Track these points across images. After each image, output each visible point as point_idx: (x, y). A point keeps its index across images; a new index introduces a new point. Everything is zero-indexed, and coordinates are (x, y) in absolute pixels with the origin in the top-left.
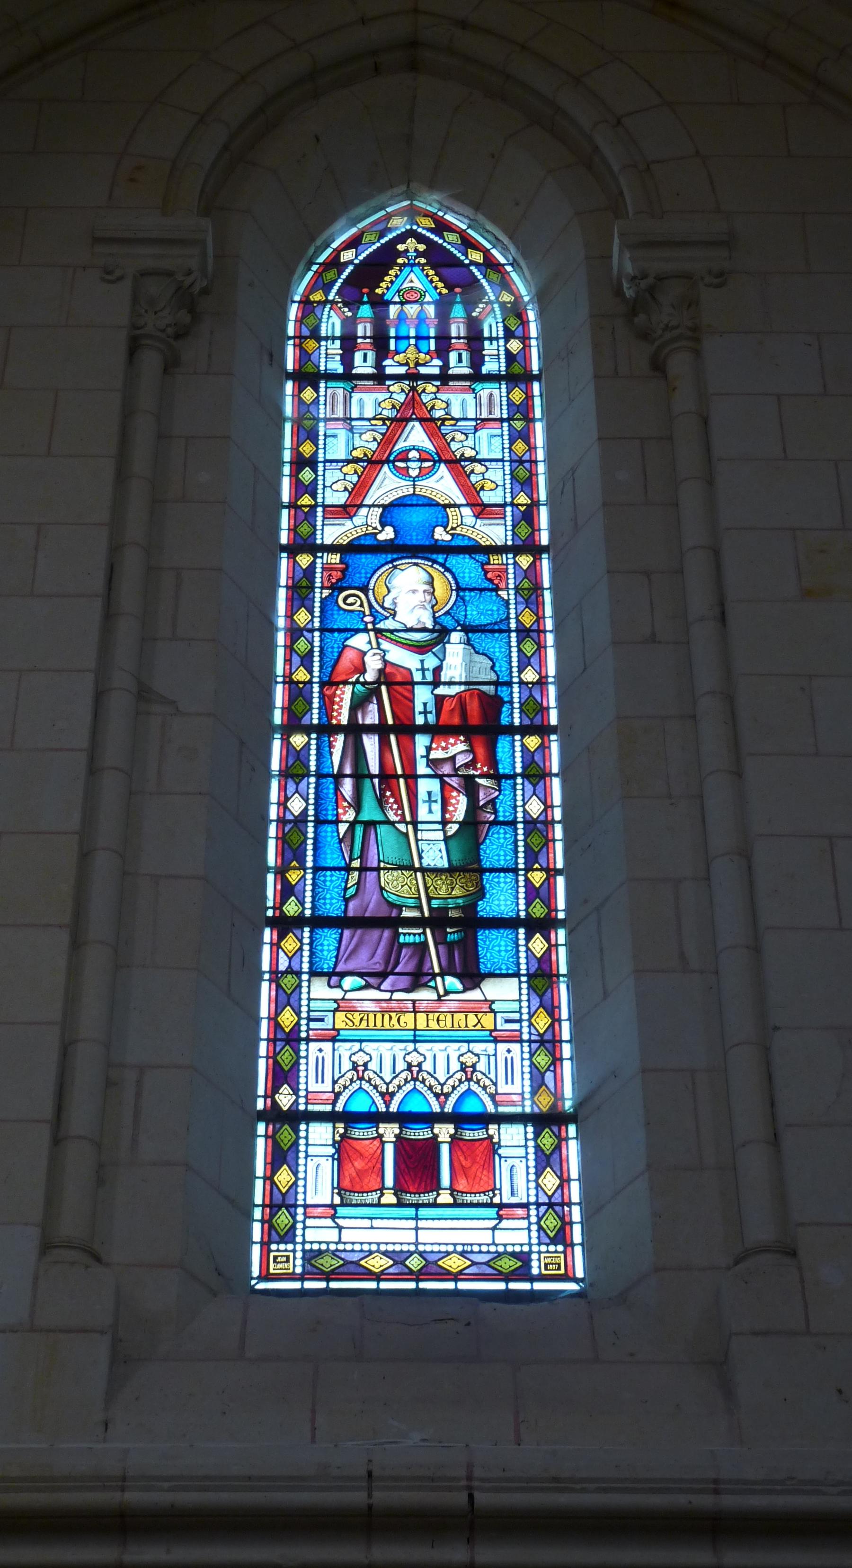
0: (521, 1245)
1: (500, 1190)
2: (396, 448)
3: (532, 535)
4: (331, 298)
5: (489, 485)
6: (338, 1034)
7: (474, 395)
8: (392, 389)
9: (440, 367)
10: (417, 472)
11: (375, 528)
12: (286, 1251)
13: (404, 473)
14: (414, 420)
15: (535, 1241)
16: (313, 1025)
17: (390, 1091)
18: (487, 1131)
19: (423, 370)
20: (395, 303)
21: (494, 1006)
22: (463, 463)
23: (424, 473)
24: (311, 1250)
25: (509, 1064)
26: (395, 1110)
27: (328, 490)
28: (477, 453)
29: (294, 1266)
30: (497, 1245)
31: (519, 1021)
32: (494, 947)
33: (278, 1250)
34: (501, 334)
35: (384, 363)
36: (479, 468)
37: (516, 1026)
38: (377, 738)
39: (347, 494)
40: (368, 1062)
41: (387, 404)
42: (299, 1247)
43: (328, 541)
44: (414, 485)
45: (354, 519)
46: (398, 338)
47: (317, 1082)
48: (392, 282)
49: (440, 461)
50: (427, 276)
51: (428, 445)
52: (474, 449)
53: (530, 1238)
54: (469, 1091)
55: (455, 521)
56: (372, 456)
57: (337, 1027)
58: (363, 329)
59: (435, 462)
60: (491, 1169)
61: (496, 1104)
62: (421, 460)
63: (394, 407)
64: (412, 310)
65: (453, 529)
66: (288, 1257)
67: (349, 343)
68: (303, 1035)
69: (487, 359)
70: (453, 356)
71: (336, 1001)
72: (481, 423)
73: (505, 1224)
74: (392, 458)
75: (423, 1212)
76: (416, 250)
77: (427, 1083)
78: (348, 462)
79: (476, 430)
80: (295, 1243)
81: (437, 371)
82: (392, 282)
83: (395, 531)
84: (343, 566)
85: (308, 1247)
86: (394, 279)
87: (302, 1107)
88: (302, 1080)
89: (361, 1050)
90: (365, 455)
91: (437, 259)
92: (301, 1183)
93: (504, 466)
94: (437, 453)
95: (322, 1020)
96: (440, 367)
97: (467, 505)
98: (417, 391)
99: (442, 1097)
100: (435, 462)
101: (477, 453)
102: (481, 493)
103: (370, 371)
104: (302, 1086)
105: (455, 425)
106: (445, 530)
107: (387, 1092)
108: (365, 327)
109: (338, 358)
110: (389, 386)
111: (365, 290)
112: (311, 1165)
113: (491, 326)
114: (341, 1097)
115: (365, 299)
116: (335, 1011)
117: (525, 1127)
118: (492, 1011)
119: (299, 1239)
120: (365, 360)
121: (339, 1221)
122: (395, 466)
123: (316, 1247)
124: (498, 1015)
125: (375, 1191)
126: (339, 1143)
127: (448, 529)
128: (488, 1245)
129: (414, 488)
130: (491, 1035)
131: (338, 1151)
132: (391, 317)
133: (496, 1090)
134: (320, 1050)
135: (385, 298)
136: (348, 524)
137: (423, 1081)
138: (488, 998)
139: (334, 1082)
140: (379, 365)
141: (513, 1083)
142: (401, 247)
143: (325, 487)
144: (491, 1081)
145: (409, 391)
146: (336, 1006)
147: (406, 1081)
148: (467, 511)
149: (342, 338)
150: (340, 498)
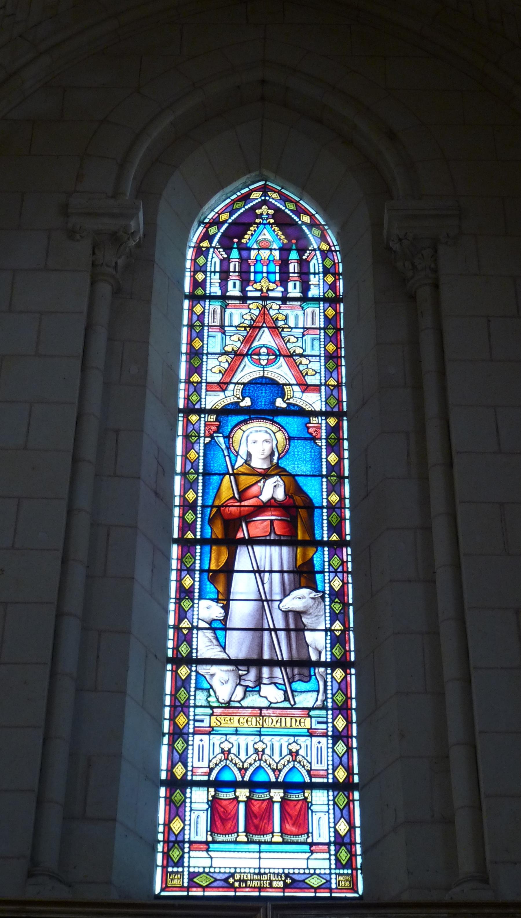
0: (325, 869)
1: (312, 833)
4: (213, 245)
5: (311, 372)
11: (239, 398)
13: (258, 362)
16: (197, 724)
20: (254, 249)
23: (270, 363)
27: (209, 372)
30: (309, 869)
31: (326, 723)
36: (304, 361)
37: (324, 726)
41: (248, 317)
43: (208, 407)
44: (264, 370)
45: (226, 392)
47: (318, 763)
48: (252, 235)
50: (274, 231)
52: (302, 348)
53: (330, 864)
61: (311, 777)
64: (264, 254)
65: (288, 399)
69: (312, 287)
73: (315, 856)
74: (250, 353)
76: (268, 214)
79: (304, 335)
90: (233, 350)
91: (281, 221)
94: (279, 350)
97: (297, 384)
98: (267, 309)
99: (243, 770)
102: (306, 377)
107: (243, 768)
109: (218, 285)
113: (314, 264)
115: (235, 246)
119: (186, 864)
122: (251, 358)
123: (196, 870)
127: (285, 399)
128: (304, 869)
133: (311, 767)
135: (248, 245)
139: (210, 761)
141: (321, 763)
142: (258, 212)
143: (207, 370)
145: (262, 308)
146: (211, 712)
147: (221, 761)
148: (296, 388)
150: (217, 378)
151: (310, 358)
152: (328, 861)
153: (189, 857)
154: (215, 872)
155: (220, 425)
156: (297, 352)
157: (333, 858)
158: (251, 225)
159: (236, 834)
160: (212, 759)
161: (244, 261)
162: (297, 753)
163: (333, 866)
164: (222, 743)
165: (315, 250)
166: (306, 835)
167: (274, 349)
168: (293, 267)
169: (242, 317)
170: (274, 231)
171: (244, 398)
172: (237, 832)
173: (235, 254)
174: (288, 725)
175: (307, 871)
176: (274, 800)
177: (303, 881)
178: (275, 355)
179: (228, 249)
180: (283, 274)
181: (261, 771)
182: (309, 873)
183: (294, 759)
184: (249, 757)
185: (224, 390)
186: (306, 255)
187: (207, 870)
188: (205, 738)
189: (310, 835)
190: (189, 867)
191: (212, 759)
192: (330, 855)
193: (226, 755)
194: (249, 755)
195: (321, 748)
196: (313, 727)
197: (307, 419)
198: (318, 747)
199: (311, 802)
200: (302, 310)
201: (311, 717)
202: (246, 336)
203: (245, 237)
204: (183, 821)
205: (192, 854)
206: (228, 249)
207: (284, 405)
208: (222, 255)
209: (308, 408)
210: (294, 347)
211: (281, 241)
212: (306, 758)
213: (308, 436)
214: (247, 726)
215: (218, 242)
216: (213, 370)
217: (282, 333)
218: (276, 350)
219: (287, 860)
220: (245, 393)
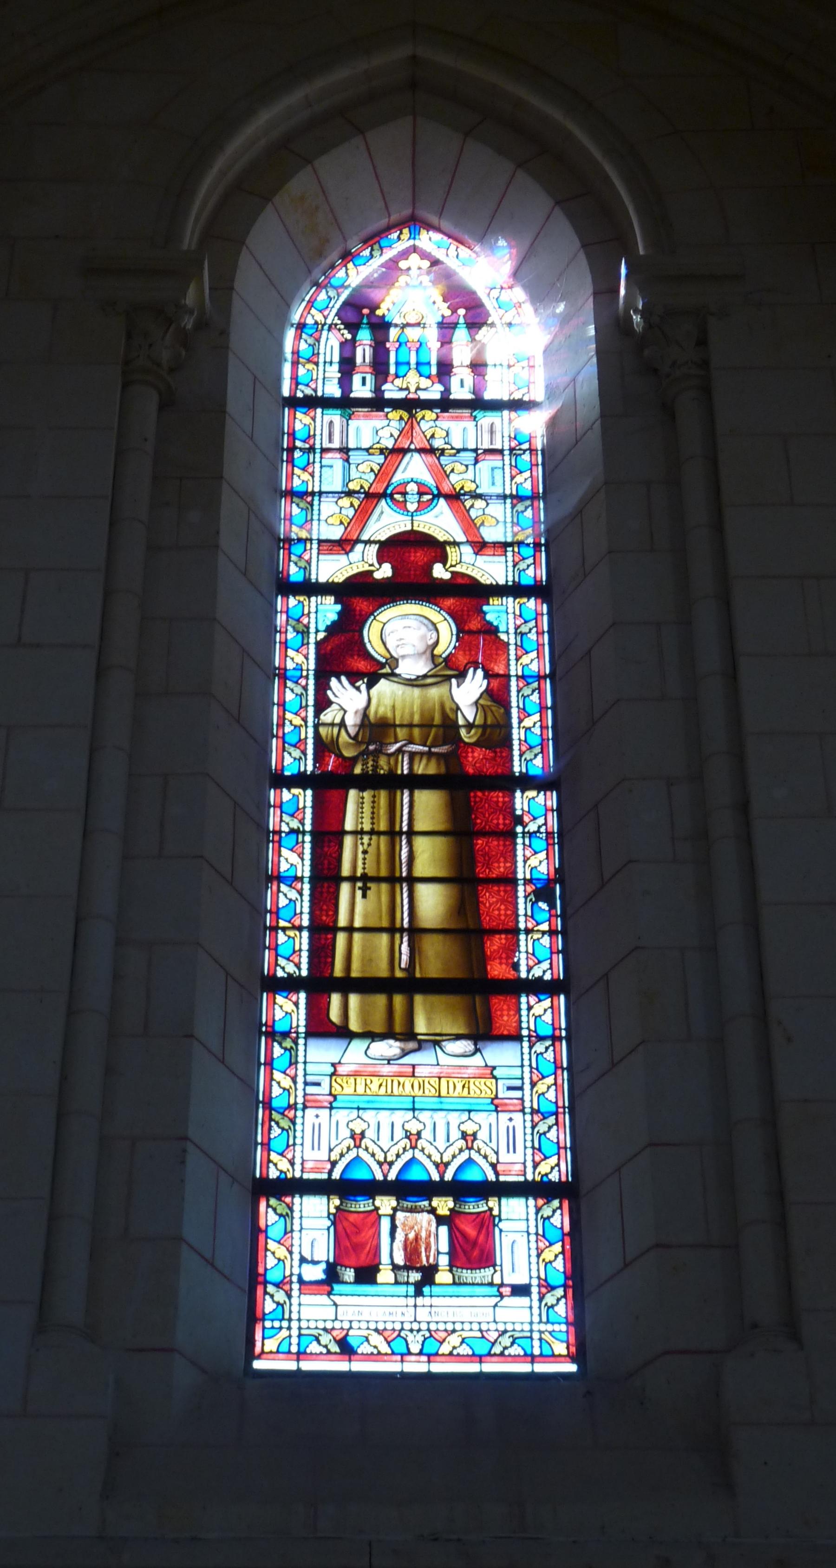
1: (501, 1266)
2: (394, 480)
8: (390, 416)
9: (442, 392)
10: (416, 505)
13: (402, 506)
14: (412, 451)
15: (536, 1319)
16: (310, 1090)
17: (389, 1159)
18: (487, 1204)
19: (423, 395)
20: (396, 325)
21: (495, 1073)
22: (462, 497)
23: (422, 507)
25: (511, 1133)
26: (338, 1178)
27: (323, 523)
28: (477, 487)
31: (521, 1088)
35: (383, 388)
36: (480, 504)
37: (518, 1094)
39: (342, 528)
43: (322, 579)
44: (412, 520)
45: (351, 554)
47: (508, 1152)
49: (440, 495)
51: (429, 480)
52: (474, 482)
54: (413, 1160)
56: (369, 488)
58: (363, 353)
59: (434, 496)
61: (497, 1174)
62: (420, 494)
67: (347, 366)
70: (454, 382)
72: (479, 454)
74: (389, 492)
79: (477, 461)
81: (437, 396)
87: (298, 1174)
90: (362, 487)
94: (437, 487)
95: (318, 1084)
96: (442, 392)
98: (416, 419)
101: (477, 487)
103: (369, 395)
105: (455, 455)
106: (444, 566)
108: (364, 350)
109: (336, 381)
110: (388, 413)
114: (337, 1166)
115: (365, 321)
116: (332, 1075)
117: (527, 1199)
118: (494, 1077)
120: (364, 383)
121: (336, 1299)
126: (334, 1215)
127: (448, 565)
129: (412, 523)
130: (492, 1103)
131: (334, 1223)
132: (391, 339)
133: (498, 1159)
134: (317, 1116)
136: (342, 559)
137: (479, 1151)
139: (331, 1150)
140: (378, 390)
141: (514, 1152)
142: (403, 264)
145: (408, 419)
146: (332, 1070)
147: (461, 1150)
148: (467, 550)
150: (336, 533)
156: (466, 489)
171: (380, 564)
176: (380, 1212)
178: (429, 496)
179: (353, 327)
183: (358, 1143)
187: (329, 1325)
189: (498, 1268)
195: (514, 1128)
198: (508, 1128)
199: (499, 1216)
205: (305, 1299)
206: (353, 327)
207: (447, 576)
209: (485, 580)
215: (337, 315)
216: (330, 521)
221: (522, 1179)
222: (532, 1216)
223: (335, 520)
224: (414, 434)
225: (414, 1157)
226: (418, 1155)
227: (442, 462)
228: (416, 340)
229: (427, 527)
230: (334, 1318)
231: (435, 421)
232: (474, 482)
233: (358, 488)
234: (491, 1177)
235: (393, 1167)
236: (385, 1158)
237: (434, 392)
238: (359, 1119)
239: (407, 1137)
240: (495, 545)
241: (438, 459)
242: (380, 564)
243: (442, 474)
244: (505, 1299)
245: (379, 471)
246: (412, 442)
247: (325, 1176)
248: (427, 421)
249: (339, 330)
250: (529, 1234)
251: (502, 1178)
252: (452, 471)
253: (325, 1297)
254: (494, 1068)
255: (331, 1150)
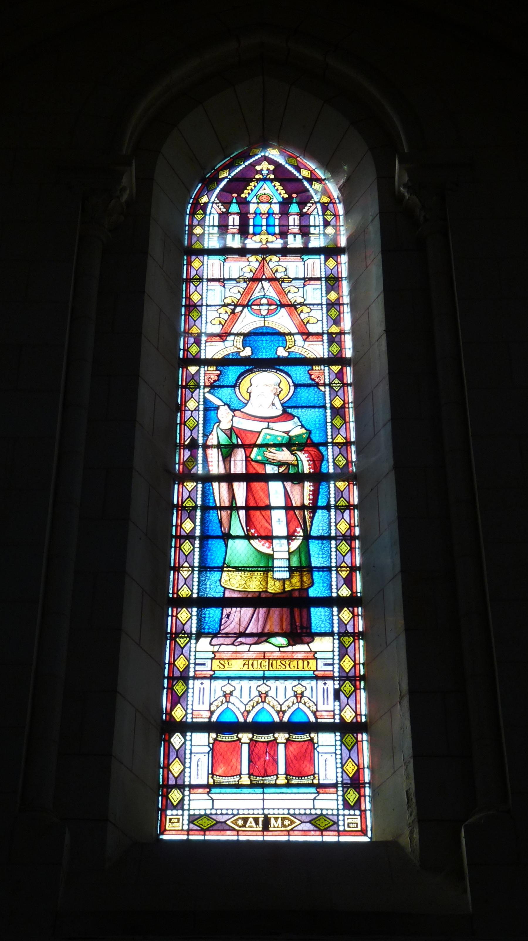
0: (332, 810)
1: (318, 774)
3: (340, 351)
4: (212, 200)
6: (214, 674)
7: (303, 263)
8: (250, 259)
11: (238, 349)
12: (177, 815)
13: (259, 313)
16: (198, 668)
19: (270, 246)
21: (316, 656)
23: (270, 313)
24: (194, 815)
27: (209, 324)
29: (183, 825)
30: (316, 809)
31: (333, 664)
32: (319, 617)
33: (172, 815)
34: (322, 223)
36: (306, 309)
37: (330, 668)
38: (245, 483)
40: (267, 692)
41: (247, 269)
42: (186, 813)
43: (209, 356)
44: (264, 320)
45: (226, 342)
46: (254, 226)
47: (324, 704)
50: (275, 186)
52: (303, 297)
53: (338, 805)
55: (291, 343)
56: (237, 302)
57: (213, 669)
58: (234, 220)
60: (312, 761)
61: (316, 718)
63: (251, 271)
64: (264, 208)
66: (179, 819)
67: (223, 227)
68: (191, 674)
71: (213, 652)
72: (307, 280)
73: (321, 796)
74: (250, 304)
75: (266, 790)
76: (268, 170)
77: (307, 705)
78: (223, 306)
79: (304, 286)
80: (183, 810)
82: (252, 190)
83: (252, 350)
84: (219, 372)
85: (192, 812)
86: (253, 188)
87: (189, 720)
88: (190, 703)
89: (299, 684)
91: (281, 175)
92: (187, 770)
93: (322, 308)
94: (280, 301)
95: (204, 664)
98: (266, 261)
100: (278, 305)
102: (308, 325)
104: (190, 707)
107: (281, 711)
111: (235, 195)
112: (194, 759)
115: (234, 201)
116: (212, 659)
119: (186, 807)
121: (214, 796)
122: (251, 308)
123: (197, 812)
124: (318, 660)
125: (236, 775)
128: (310, 809)
129: (264, 322)
131: (212, 749)
138: (313, 650)
139: (211, 704)
141: (328, 704)
142: (258, 168)
143: (206, 322)
144: (314, 703)
145: (261, 261)
148: (298, 338)
149: (219, 226)
150: (217, 329)
151: (311, 307)
152: (336, 801)
153: (190, 800)
154: (216, 814)
155: (220, 374)
156: (298, 301)
157: (340, 798)
158: (251, 180)
159: (238, 776)
160: (213, 702)
161: (244, 217)
162: (266, 694)
163: (341, 807)
164: (259, 686)
165: (316, 203)
166: (238, 776)
167: (275, 299)
168: (294, 220)
169: (242, 269)
170: (275, 186)
171: (244, 348)
172: (277, 775)
173: (234, 208)
174: (300, 667)
175: (313, 812)
176: (278, 741)
177: (225, 822)
179: (227, 204)
180: (225, 224)
181: (265, 713)
182: (232, 814)
183: (263, 700)
184: (287, 700)
185: (224, 341)
186: (307, 208)
188: (207, 682)
190: (189, 810)
191: (213, 702)
192: (338, 796)
193: (299, 699)
194: (287, 698)
195: (204, 689)
196: (318, 669)
197: (310, 367)
198: (200, 688)
200: (303, 261)
201: (316, 659)
202: (246, 288)
203: (245, 191)
204: (184, 763)
205: (193, 797)
206: (227, 204)
208: (220, 209)
210: (294, 296)
211: (282, 196)
212: (312, 699)
213: (310, 382)
214: (252, 669)
215: (216, 197)
216: (213, 322)
217: (283, 284)
218: (276, 301)
219: (301, 801)
220: (246, 344)
221: (332, 721)
222: (339, 743)
223: (216, 322)
224: (265, 270)
225: (263, 708)
226: (302, 706)
227: (283, 286)
228: (266, 212)
229: (280, 327)
230: (211, 807)
231: (278, 262)
232: (303, 297)
233: (230, 302)
234: (312, 719)
235: (286, 714)
236: (281, 708)
237: (278, 244)
238: (229, 685)
239: (260, 696)
240: (317, 334)
241: (281, 285)
242: (244, 348)
243: (282, 292)
244: (321, 795)
245: (243, 292)
246: (264, 274)
247: (207, 720)
248: (274, 260)
249: (218, 206)
250: (336, 754)
251: (319, 720)
252: (289, 291)
253: (206, 795)
254: (316, 652)
255: (211, 704)
